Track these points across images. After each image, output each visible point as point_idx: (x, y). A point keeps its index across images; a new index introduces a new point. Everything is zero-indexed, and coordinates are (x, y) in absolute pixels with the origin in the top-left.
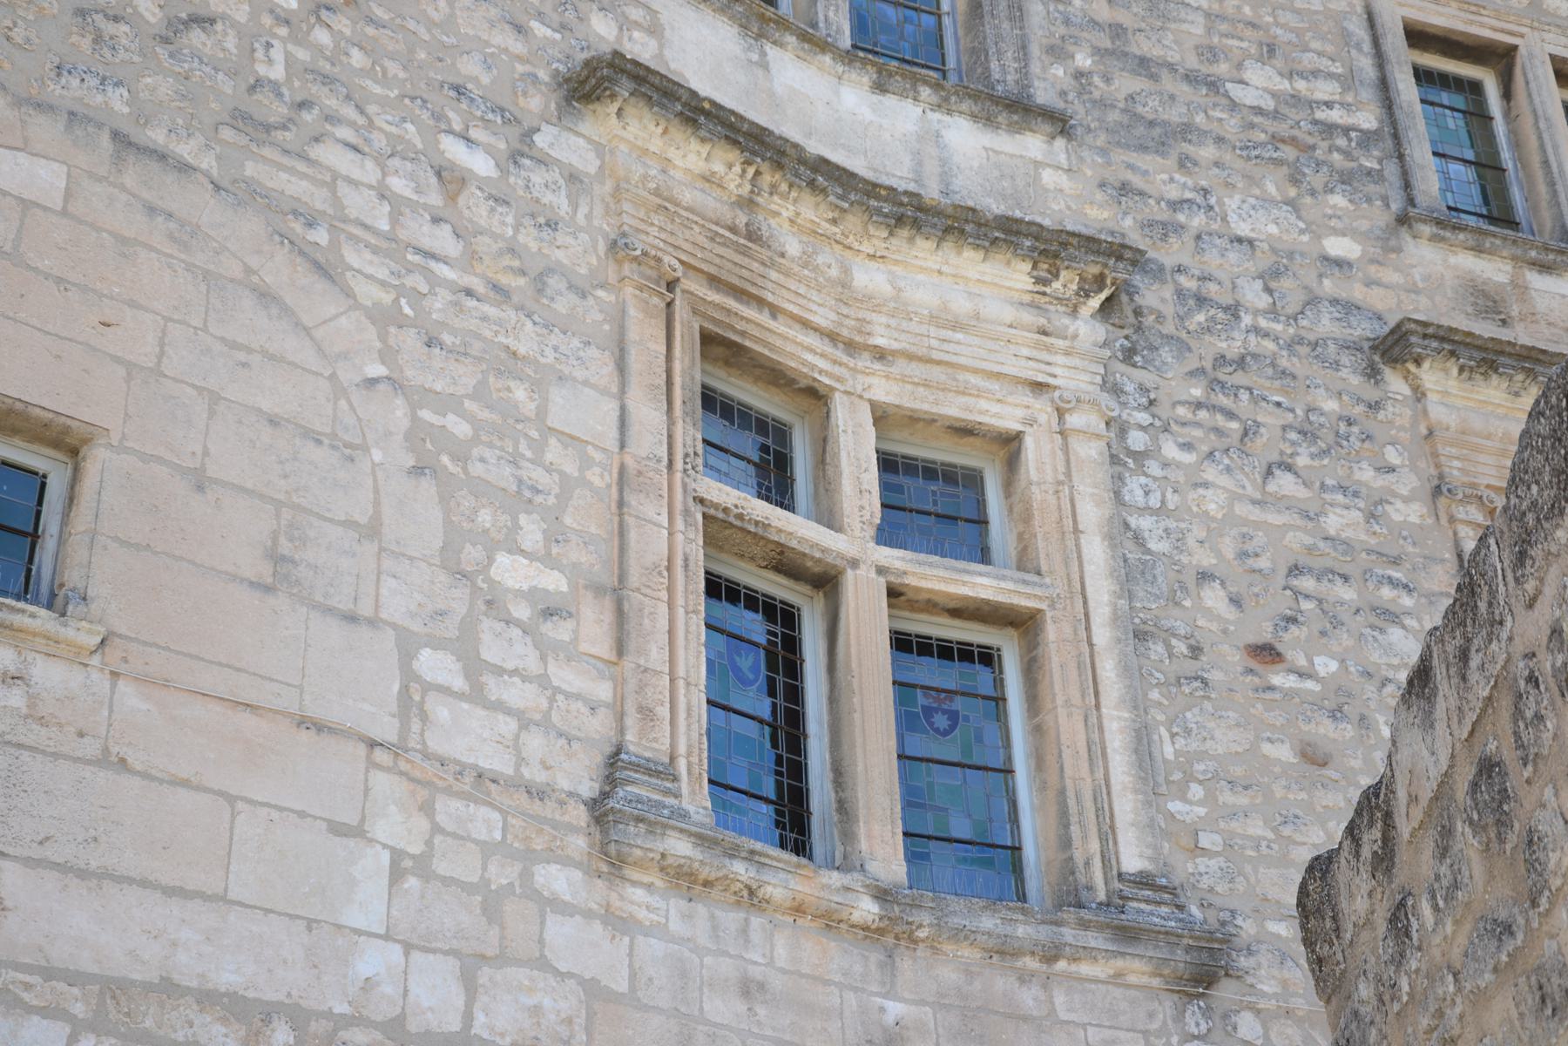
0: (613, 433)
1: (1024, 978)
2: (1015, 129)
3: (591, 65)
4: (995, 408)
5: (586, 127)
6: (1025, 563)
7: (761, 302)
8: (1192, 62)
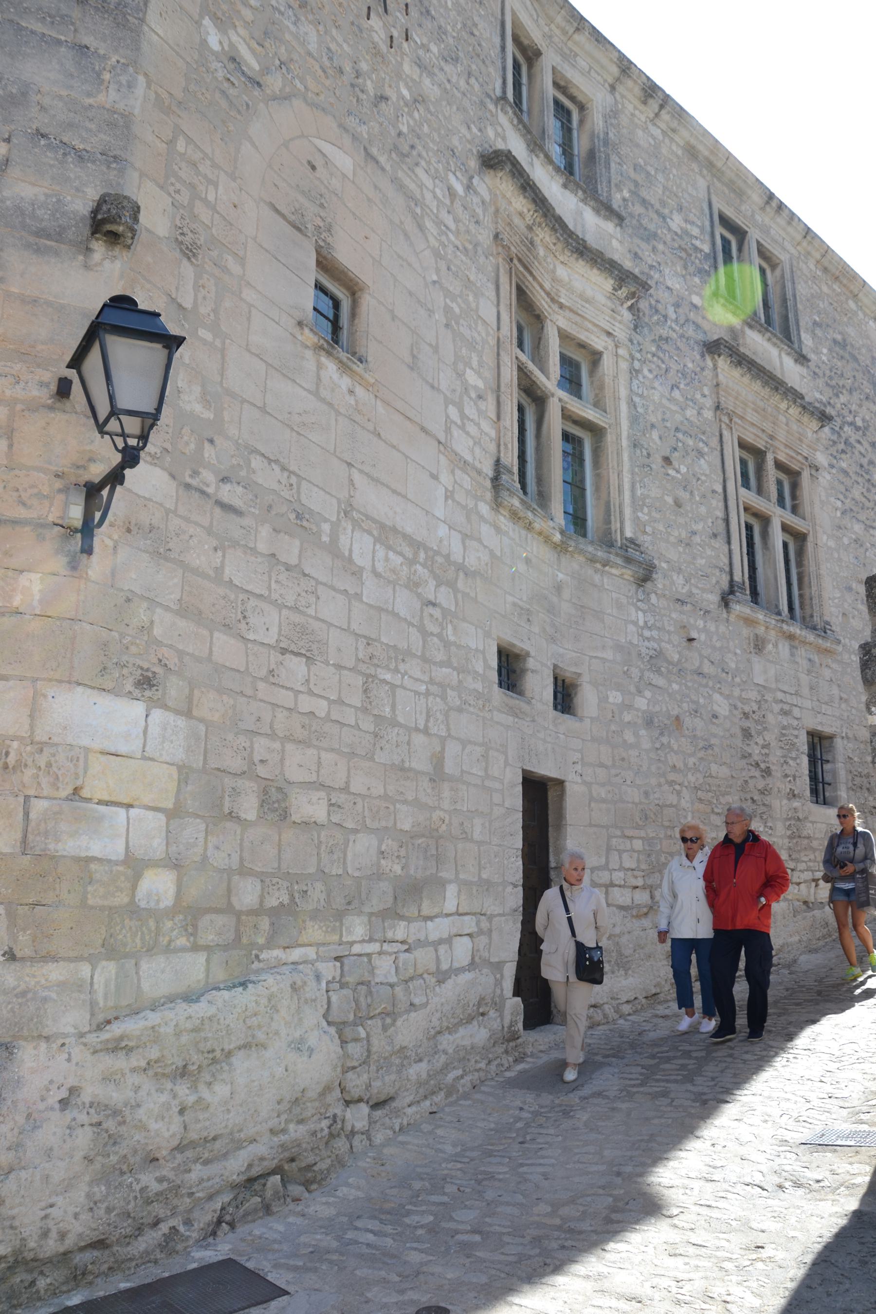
0: (495, 323)
1: (596, 571)
2: (606, 218)
3: (497, 153)
4: (596, 340)
5: (487, 179)
6: (598, 404)
7: (531, 273)
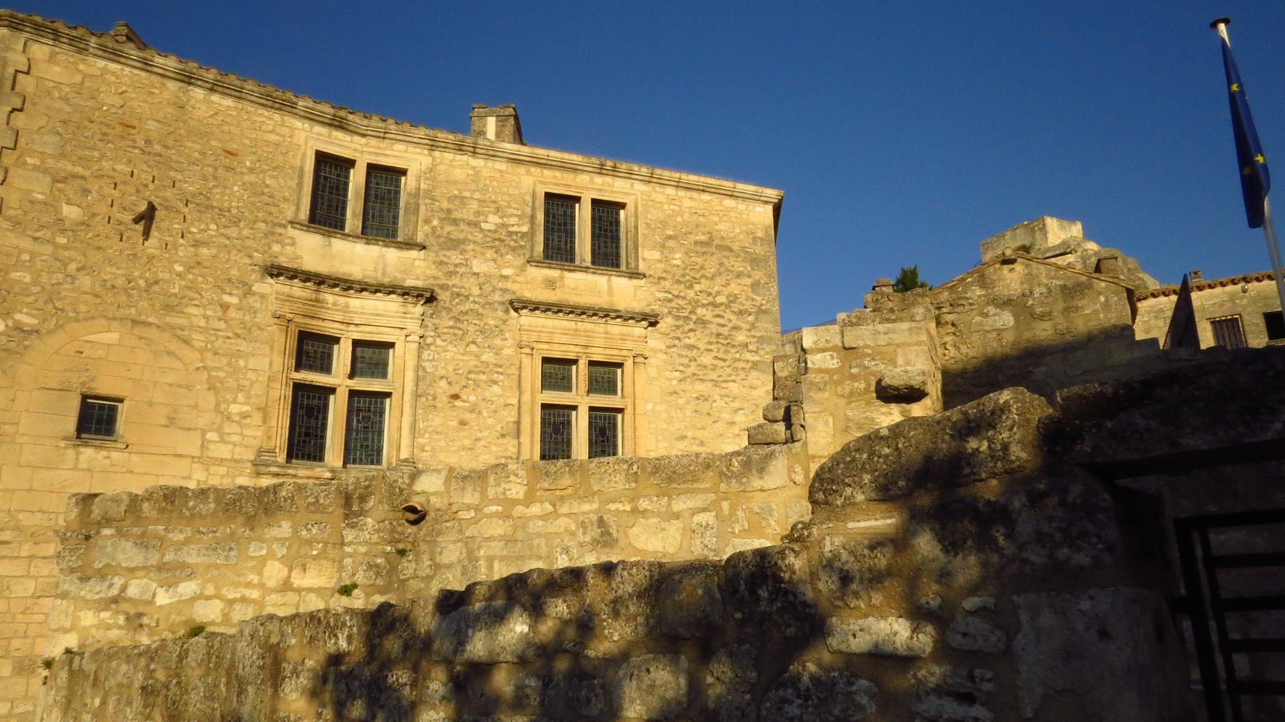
8: (471, 217)
